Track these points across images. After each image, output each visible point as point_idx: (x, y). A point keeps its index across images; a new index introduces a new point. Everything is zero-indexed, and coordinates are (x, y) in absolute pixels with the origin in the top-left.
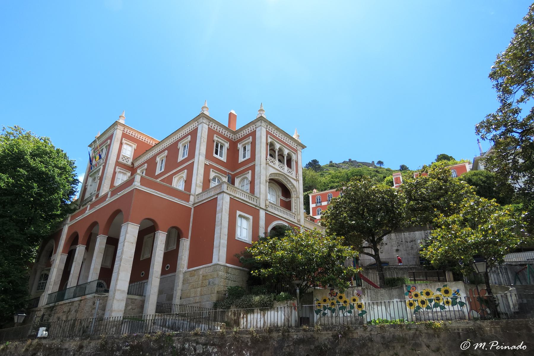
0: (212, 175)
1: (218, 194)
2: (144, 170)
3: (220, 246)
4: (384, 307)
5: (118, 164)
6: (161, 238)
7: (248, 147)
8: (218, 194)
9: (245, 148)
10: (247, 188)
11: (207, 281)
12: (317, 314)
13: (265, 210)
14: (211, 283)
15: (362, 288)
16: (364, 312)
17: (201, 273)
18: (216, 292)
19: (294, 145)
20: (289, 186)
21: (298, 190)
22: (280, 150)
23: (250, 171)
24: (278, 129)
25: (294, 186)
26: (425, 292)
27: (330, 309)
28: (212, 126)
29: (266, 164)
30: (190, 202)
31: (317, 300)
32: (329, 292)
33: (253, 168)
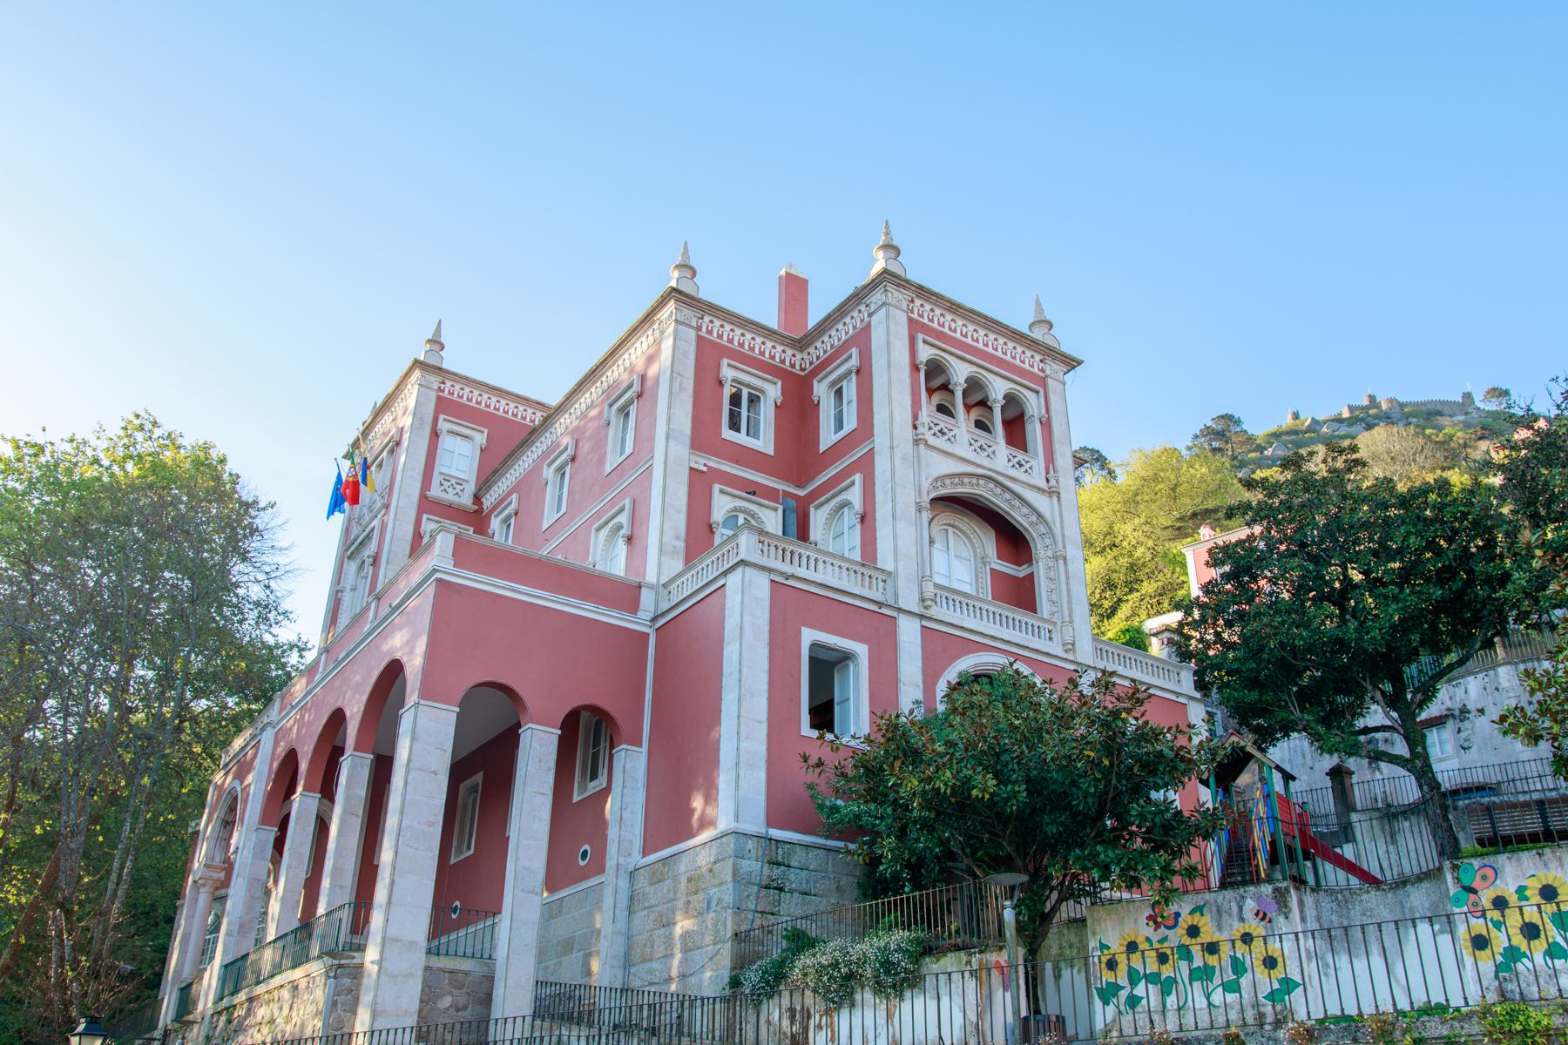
0: (722, 504)
1: (725, 573)
2: (509, 517)
3: (738, 764)
4: (1377, 962)
5: (427, 504)
6: (538, 749)
7: (850, 389)
8: (725, 573)
9: (839, 393)
10: (851, 543)
11: (701, 895)
12: (1106, 1002)
13: (922, 617)
14: (714, 902)
15: (1276, 890)
16: (1288, 985)
17: (682, 868)
18: (729, 933)
19: (1029, 360)
20: (1019, 517)
21: (1057, 531)
22: (973, 384)
23: (858, 478)
24: (954, 308)
25: (1040, 515)
26: (1534, 886)
27: (1153, 978)
28: (710, 332)
29: (916, 442)
30: (641, 614)
31: (1103, 946)
32: (1149, 912)
33: (866, 466)
